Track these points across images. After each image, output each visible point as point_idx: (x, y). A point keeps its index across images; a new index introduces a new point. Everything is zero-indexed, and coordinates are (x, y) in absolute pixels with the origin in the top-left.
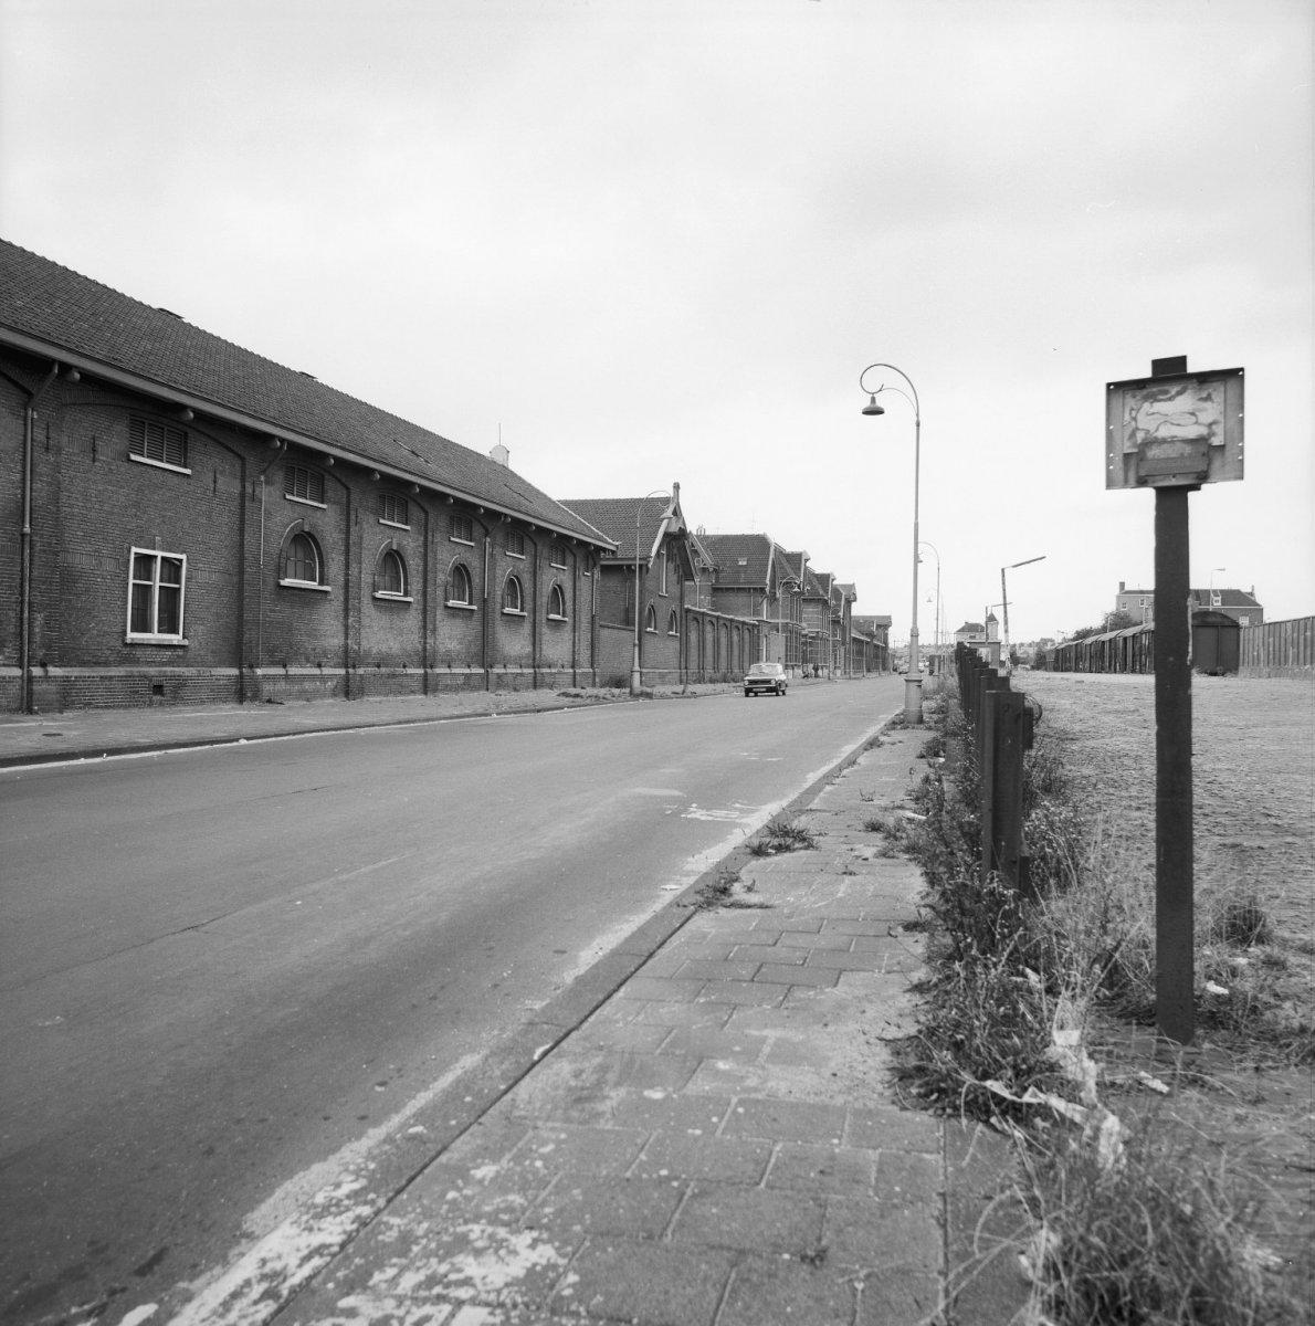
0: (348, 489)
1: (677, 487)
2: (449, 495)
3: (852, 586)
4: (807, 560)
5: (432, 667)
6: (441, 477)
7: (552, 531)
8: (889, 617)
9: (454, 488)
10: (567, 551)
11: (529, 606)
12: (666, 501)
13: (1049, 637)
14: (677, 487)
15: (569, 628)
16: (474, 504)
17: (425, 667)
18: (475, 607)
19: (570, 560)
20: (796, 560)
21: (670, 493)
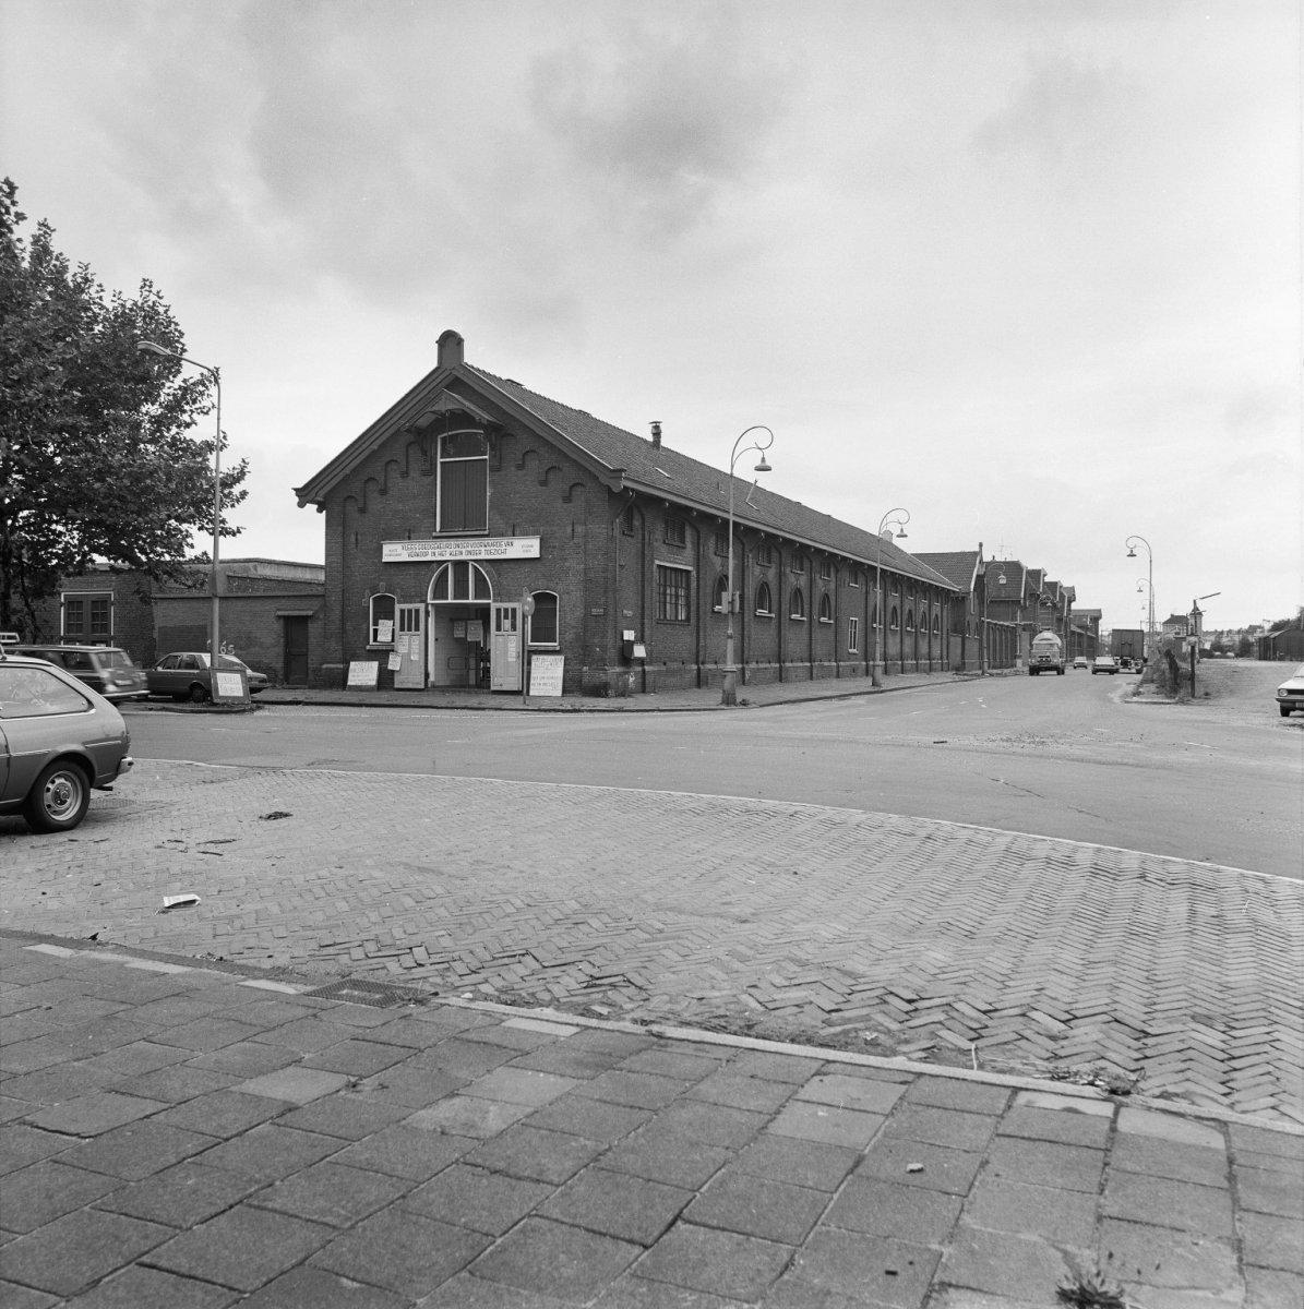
0: (743, 544)
1: (981, 545)
2: (665, 500)
3: (1073, 589)
4: (1045, 575)
5: (703, 663)
6: (701, 501)
7: (665, 500)
8: (1100, 611)
9: (696, 501)
10: (773, 550)
11: (775, 608)
12: (975, 554)
13: (1258, 624)
14: (981, 545)
15: (806, 626)
16: (687, 507)
17: (742, 663)
18: (773, 615)
19: (806, 564)
20: (1036, 575)
21: (977, 549)
